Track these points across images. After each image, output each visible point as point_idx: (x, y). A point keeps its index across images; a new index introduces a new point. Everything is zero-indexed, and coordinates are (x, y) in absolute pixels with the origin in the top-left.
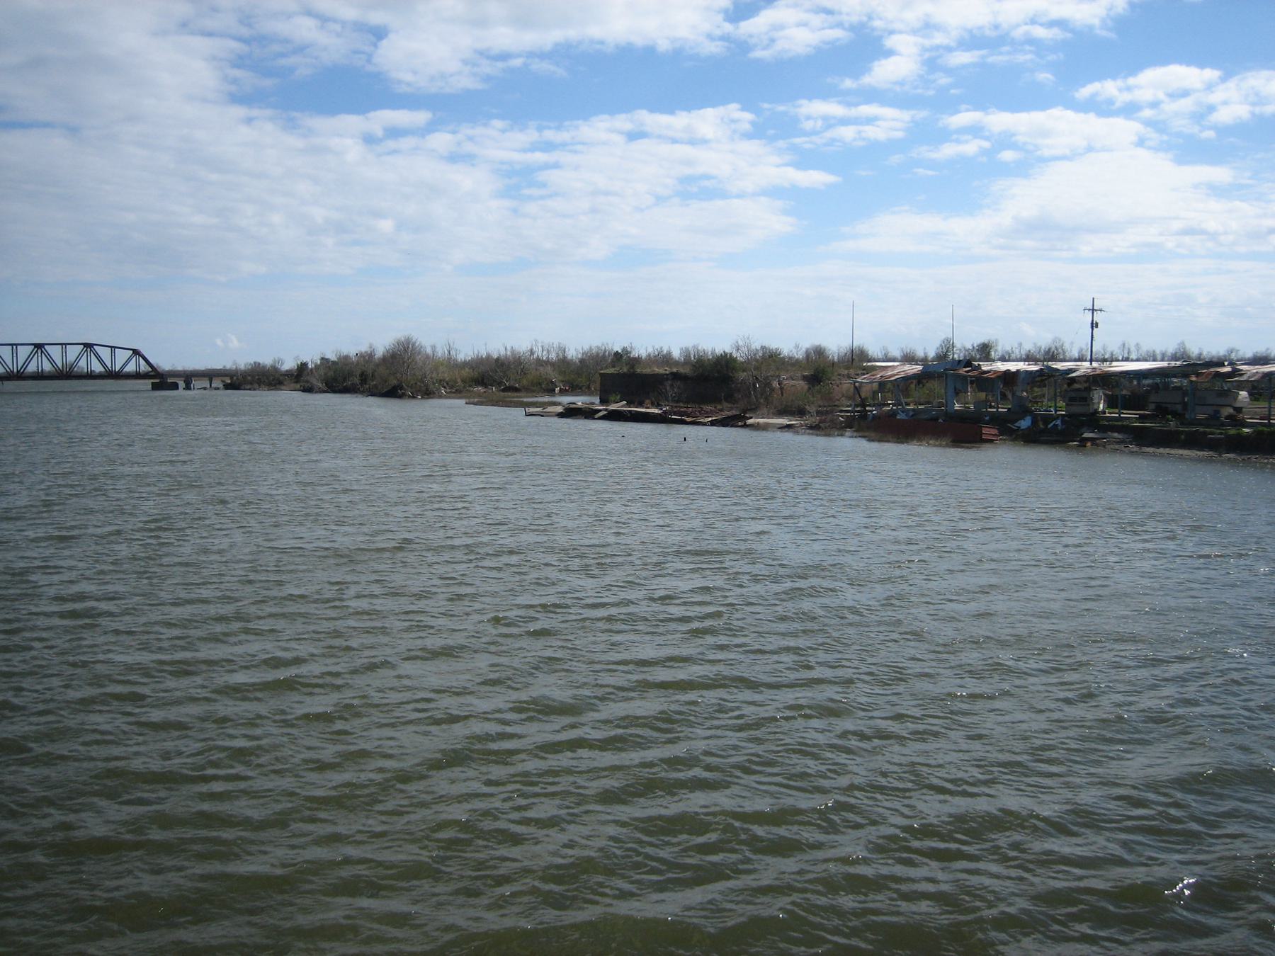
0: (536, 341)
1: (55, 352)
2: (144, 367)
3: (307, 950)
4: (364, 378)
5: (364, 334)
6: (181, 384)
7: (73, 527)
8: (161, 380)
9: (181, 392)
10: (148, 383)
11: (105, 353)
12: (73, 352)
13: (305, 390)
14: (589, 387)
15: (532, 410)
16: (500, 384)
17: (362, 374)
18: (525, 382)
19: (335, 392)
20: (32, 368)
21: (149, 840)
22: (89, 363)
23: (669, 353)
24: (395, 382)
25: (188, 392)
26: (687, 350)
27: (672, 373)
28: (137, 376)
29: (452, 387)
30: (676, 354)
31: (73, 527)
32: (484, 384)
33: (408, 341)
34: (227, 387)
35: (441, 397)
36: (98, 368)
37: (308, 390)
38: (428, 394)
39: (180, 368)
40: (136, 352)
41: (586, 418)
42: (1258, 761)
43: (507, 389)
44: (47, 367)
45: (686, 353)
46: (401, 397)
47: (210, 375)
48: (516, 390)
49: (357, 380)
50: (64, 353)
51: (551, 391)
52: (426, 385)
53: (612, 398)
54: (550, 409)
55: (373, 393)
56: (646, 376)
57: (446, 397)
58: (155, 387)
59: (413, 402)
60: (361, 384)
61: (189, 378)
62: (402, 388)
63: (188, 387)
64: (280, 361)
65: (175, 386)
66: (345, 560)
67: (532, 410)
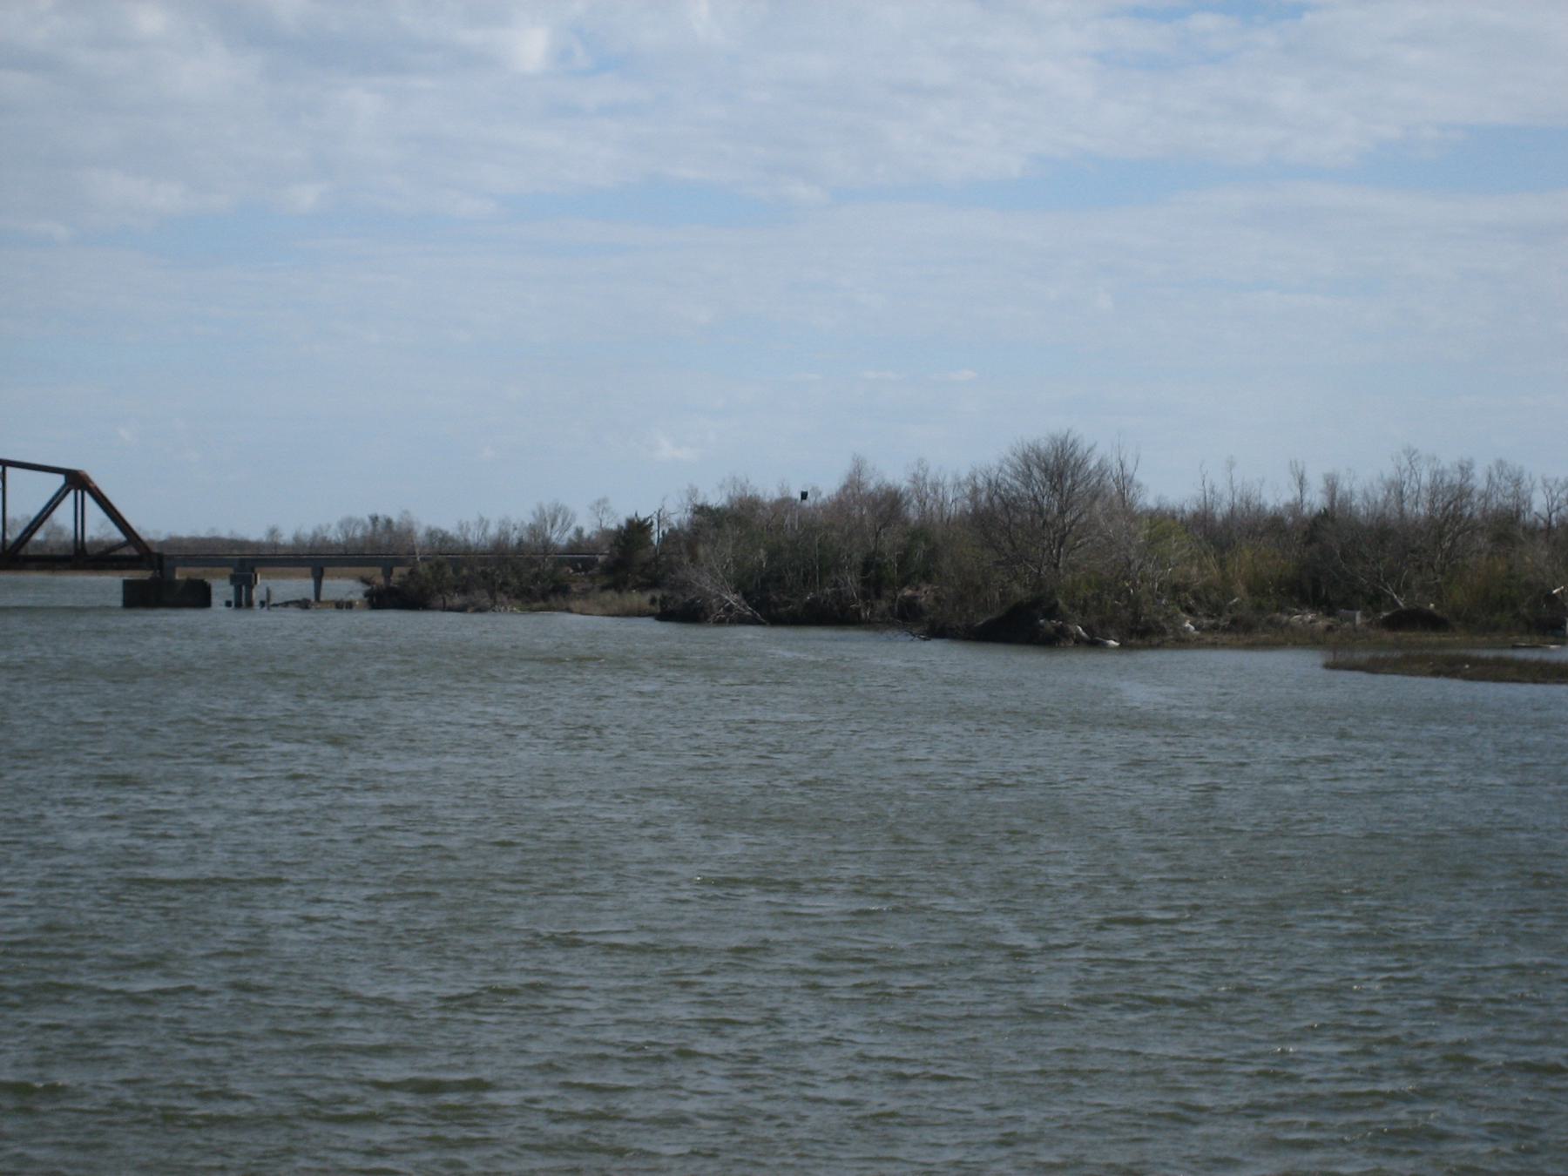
2: (98, 528)
3: (222, 1168)
4: (874, 577)
6: (222, 589)
7: (10, 884)
8: (162, 577)
9: (219, 615)
10: (111, 583)
16: (1375, 600)
17: (867, 565)
19: (775, 620)
22: (80, 515)
24: (1020, 592)
25: (243, 619)
26: (349, 521)
28: (82, 557)
29: (1216, 610)
30: (420, 533)
31: (10, 884)
32: (1326, 606)
34: (380, 599)
35: (1182, 642)
37: (690, 613)
39: (286, 537)
40: (77, 481)
43: (1400, 621)
45: (431, 534)
46: (1050, 641)
47: (315, 559)
48: (1434, 623)
49: (851, 582)
52: (1134, 603)
57: (1199, 644)
58: (136, 597)
60: (864, 596)
61: (245, 564)
62: (1052, 612)
63: (242, 602)
64: (558, 514)
65: (199, 596)
66: (870, 966)
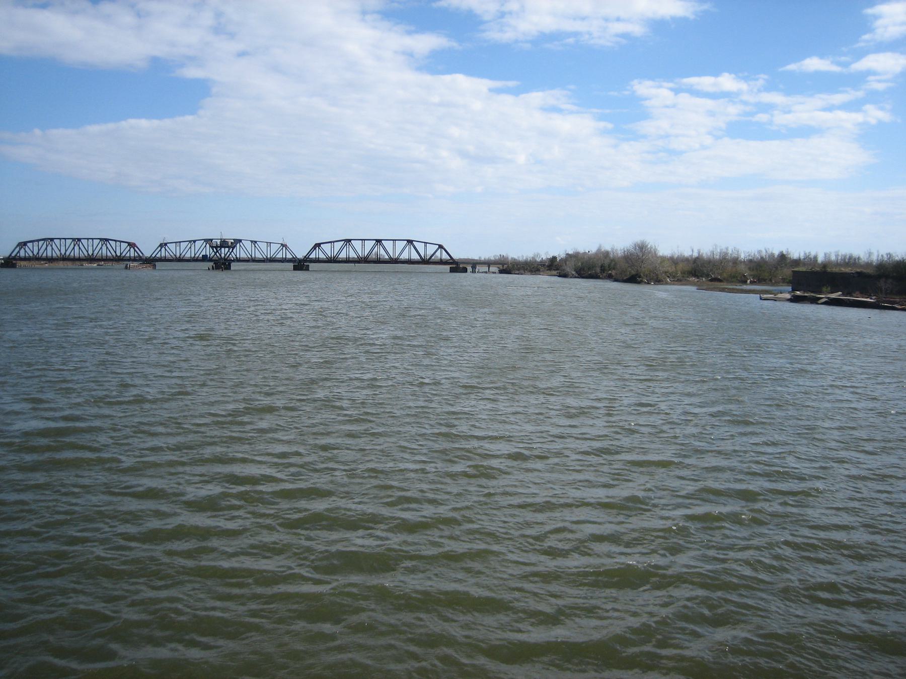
0: (716, 245)
1: (388, 245)
2: (445, 256)
4: (603, 269)
5: (616, 240)
6: (469, 269)
8: (457, 266)
10: (447, 268)
11: (421, 248)
12: (431, 249)
13: (560, 276)
14: (771, 280)
15: (765, 296)
16: (707, 276)
17: (602, 266)
18: (725, 275)
20: (343, 255)
21: (294, 574)
23: (816, 257)
24: (633, 273)
27: (857, 273)
28: (441, 262)
29: (674, 277)
30: (821, 259)
32: (695, 275)
33: (642, 247)
34: (501, 272)
35: (667, 283)
36: (415, 256)
37: (565, 276)
38: (658, 281)
39: (483, 259)
40: (441, 247)
41: (812, 303)
42: (447, 549)
44: (353, 255)
47: (488, 263)
49: (598, 270)
50: (363, 246)
51: (745, 282)
52: (657, 275)
53: (824, 289)
54: (780, 296)
55: (610, 277)
56: (836, 274)
58: (452, 270)
59: (648, 286)
61: (474, 264)
63: (474, 272)
67: (765, 296)
